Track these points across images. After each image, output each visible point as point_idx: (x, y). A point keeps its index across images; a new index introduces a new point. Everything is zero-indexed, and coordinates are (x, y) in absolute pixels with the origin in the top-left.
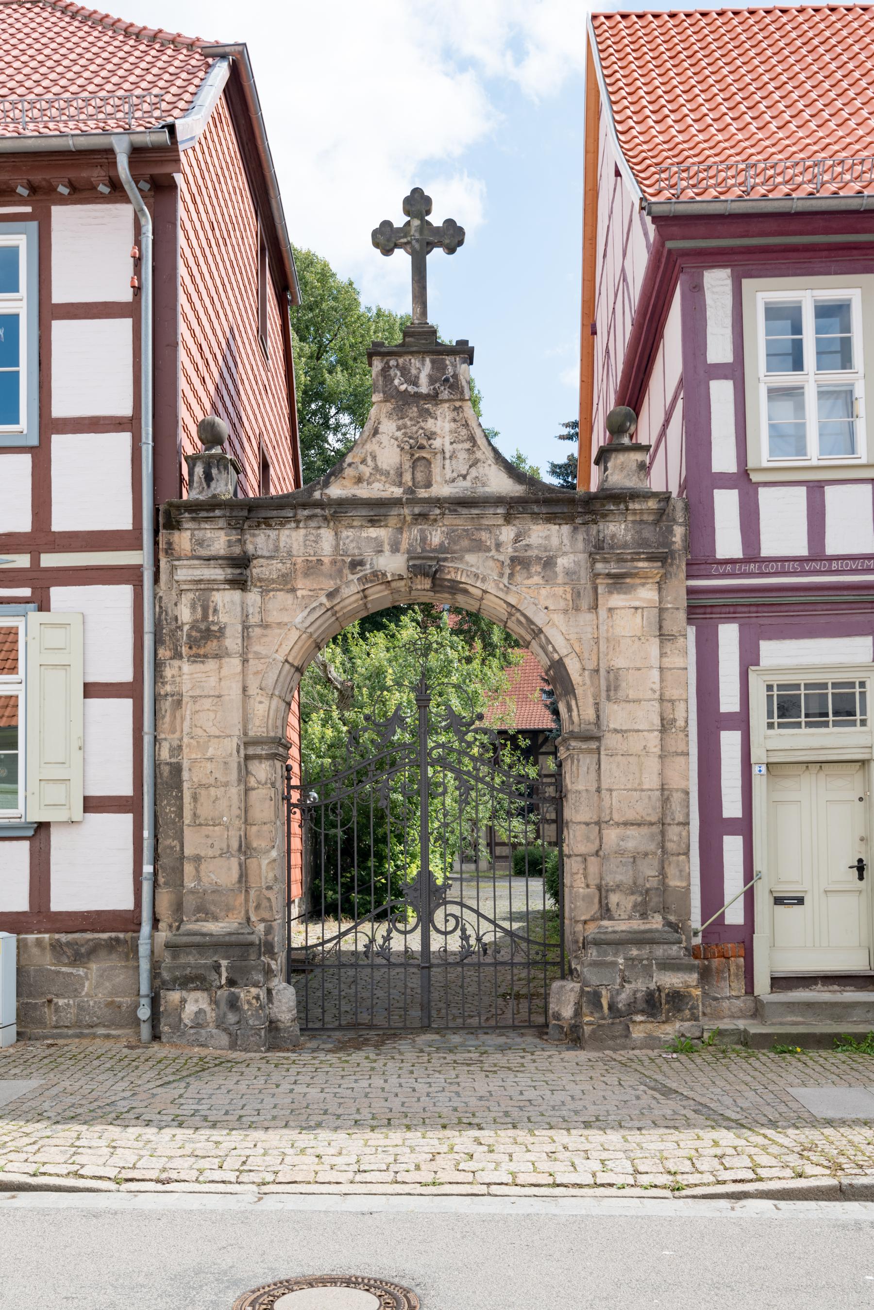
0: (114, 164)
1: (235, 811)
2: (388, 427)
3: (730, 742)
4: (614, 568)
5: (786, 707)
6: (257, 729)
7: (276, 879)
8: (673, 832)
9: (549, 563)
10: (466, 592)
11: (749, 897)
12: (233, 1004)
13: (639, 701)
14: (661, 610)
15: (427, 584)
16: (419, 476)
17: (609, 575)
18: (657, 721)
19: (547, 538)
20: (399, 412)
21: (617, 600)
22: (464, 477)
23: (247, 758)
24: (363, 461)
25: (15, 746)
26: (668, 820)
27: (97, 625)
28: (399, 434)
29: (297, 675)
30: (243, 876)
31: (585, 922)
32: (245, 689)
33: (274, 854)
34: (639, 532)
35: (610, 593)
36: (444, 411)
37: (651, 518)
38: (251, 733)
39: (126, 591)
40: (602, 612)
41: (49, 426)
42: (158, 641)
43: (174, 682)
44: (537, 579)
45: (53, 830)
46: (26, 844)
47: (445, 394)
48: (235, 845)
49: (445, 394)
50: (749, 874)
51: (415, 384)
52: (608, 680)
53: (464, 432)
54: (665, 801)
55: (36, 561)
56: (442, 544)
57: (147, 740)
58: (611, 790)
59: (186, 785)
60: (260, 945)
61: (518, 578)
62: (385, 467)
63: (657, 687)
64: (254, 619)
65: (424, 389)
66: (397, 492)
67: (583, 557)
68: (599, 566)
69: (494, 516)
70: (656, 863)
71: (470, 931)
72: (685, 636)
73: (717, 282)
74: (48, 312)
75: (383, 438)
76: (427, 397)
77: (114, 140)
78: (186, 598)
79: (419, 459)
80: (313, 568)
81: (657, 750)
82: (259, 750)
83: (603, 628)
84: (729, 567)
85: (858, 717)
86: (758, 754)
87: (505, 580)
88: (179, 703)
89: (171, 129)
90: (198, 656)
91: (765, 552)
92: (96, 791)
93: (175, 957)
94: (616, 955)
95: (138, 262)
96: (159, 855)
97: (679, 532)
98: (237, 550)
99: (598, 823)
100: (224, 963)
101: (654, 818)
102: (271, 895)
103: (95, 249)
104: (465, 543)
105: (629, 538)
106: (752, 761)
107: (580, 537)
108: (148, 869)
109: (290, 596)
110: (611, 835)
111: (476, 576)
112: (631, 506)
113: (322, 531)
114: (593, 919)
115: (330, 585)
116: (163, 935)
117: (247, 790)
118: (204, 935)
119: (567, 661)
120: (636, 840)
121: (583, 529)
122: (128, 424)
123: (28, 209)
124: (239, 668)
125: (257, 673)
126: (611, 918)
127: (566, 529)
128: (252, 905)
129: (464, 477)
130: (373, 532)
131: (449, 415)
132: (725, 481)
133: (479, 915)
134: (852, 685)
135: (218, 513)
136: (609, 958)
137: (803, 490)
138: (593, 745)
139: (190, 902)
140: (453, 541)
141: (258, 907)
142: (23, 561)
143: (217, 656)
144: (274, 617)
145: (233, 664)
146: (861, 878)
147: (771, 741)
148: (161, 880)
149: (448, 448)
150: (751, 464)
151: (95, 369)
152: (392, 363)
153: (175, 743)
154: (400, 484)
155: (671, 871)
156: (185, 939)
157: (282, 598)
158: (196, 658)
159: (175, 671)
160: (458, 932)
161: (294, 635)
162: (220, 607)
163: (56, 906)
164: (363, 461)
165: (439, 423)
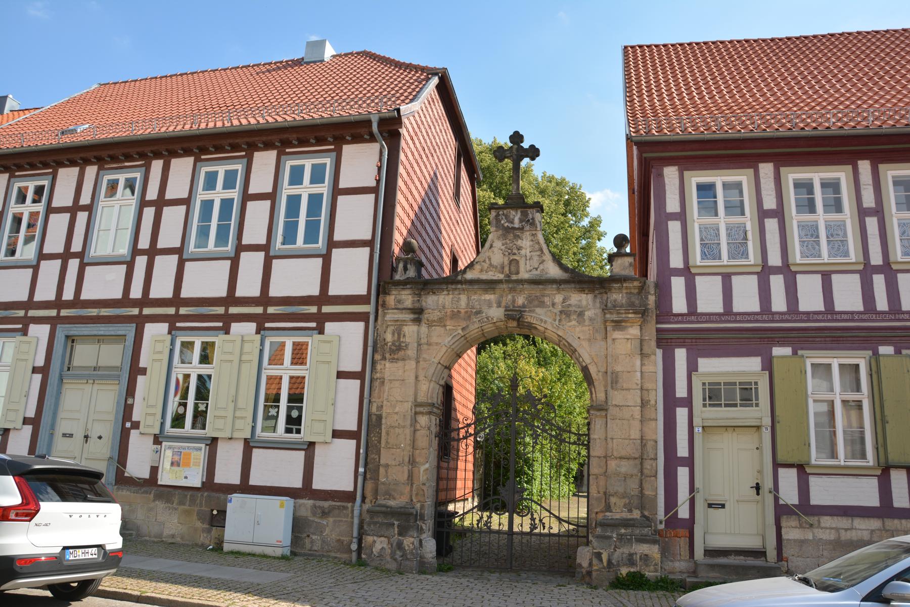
0: (371, 126)
1: (408, 442)
2: (498, 244)
3: (682, 414)
4: (615, 317)
5: (713, 395)
6: (421, 398)
7: (428, 479)
8: (648, 465)
9: (581, 314)
10: (536, 328)
11: (692, 502)
12: (400, 546)
13: (628, 389)
14: (642, 341)
15: (515, 324)
16: (513, 269)
17: (613, 321)
18: (639, 401)
19: (580, 301)
20: (504, 236)
21: (617, 335)
22: (536, 269)
23: (416, 413)
24: (484, 261)
25: (302, 402)
26: (645, 457)
27: (347, 341)
28: (503, 247)
29: (446, 371)
30: (411, 476)
31: (597, 513)
32: (417, 377)
33: (427, 466)
34: (629, 298)
35: (614, 330)
36: (527, 235)
37: (636, 291)
38: (419, 400)
39: (361, 325)
40: (609, 340)
41: (332, 244)
42: (375, 351)
43: (381, 372)
44: (574, 323)
45: (317, 446)
46: (303, 453)
47: (527, 228)
48: (407, 460)
49: (527, 228)
50: (692, 489)
51: (512, 223)
52: (612, 378)
53: (537, 246)
54: (643, 445)
55: (320, 309)
56: (523, 304)
57: (366, 401)
58: (612, 439)
59: (383, 426)
60: (416, 515)
61: (564, 322)
62: (495, 264)
63: (639, 382)
64: (424, 341)
65: (517, 225)
66: (501, 276)
67: (599, 311)
68: (608, 316)
69: (550, 290)
70: (637, 481)
71: (535, 516)
72: (655, 354)
73: (671, 174)
74: (337, 191)
75: (495, 249)
76: (518, 229)
77: (371, 116)
78: (390, 330)
79: (513, 260)
80: (455, 315)
81: (639, 417)
82: (421, 409)
83: (610, 349)
84: (680, 318)
85: (754, 402)
86: (697, 421)
87: (557, 322)
88: (383, 383)
89: (398, 110)
90: (393, 359)
91: (699, 310)
92: (339, 427)
93: (371, 518)
94: (612, 532)
95: (380, 169)
96: (368, 464)
97: (652, 299)
98: (417, 305)
99: (605, 457)
100: (396, 523)
101: (637, 455)
102: (425, 488)
103: (360, 163)
104: (536, 303)
105: (624, 301)
106: (694, 425)
107: (598, 300)
108: (361, 470)
109: (442, 329)
110: (612, 464)
111: (541, 320)
112: (625, 285)
113: (461, 296)
114: (602, 512)
115: (464, 324)
116: (367, 506)
117: (415, 431)
118: (387, 507)
119: (590, 367)
120: (626, 467)
121: (599, 296)
122: (369, 243)
123: (332, 147)
124: (414, 366)
125: (423, 369)
126: (611, 512)
127: (590, 296)
128: (414, 493)
129: (536, 269)
130: (487, 297)
131: (529, 238)
132: (677, 272)
133: (541, 506)
134: (750, 383)
135: (408, 286)
136: (608, 534)
137: (720, 278)
138: (603, 413)
139: (382, 488)
140: (530, 302)
141: (417, 494)
142: (313, 309)
143: (404, 360)
144: (434, 339)
145: (413, 364)
146: (758, 494)
147: (704, 413)
148: (368, 476)
149: (528, 254)
150: (691, 263)
151: (356, 218)
152: (501, 213)
153: (380, 404)
154: (502, 273)
155: (646, 485)
156: (378, 509)
157: (438, 330)
158: (393, 360)
159: (382, 367)
160: (529, 516)
161: (444, 349)
162: (407, 334)
163: (315, 487)
164: (484, 261)
165: (524, 242)
